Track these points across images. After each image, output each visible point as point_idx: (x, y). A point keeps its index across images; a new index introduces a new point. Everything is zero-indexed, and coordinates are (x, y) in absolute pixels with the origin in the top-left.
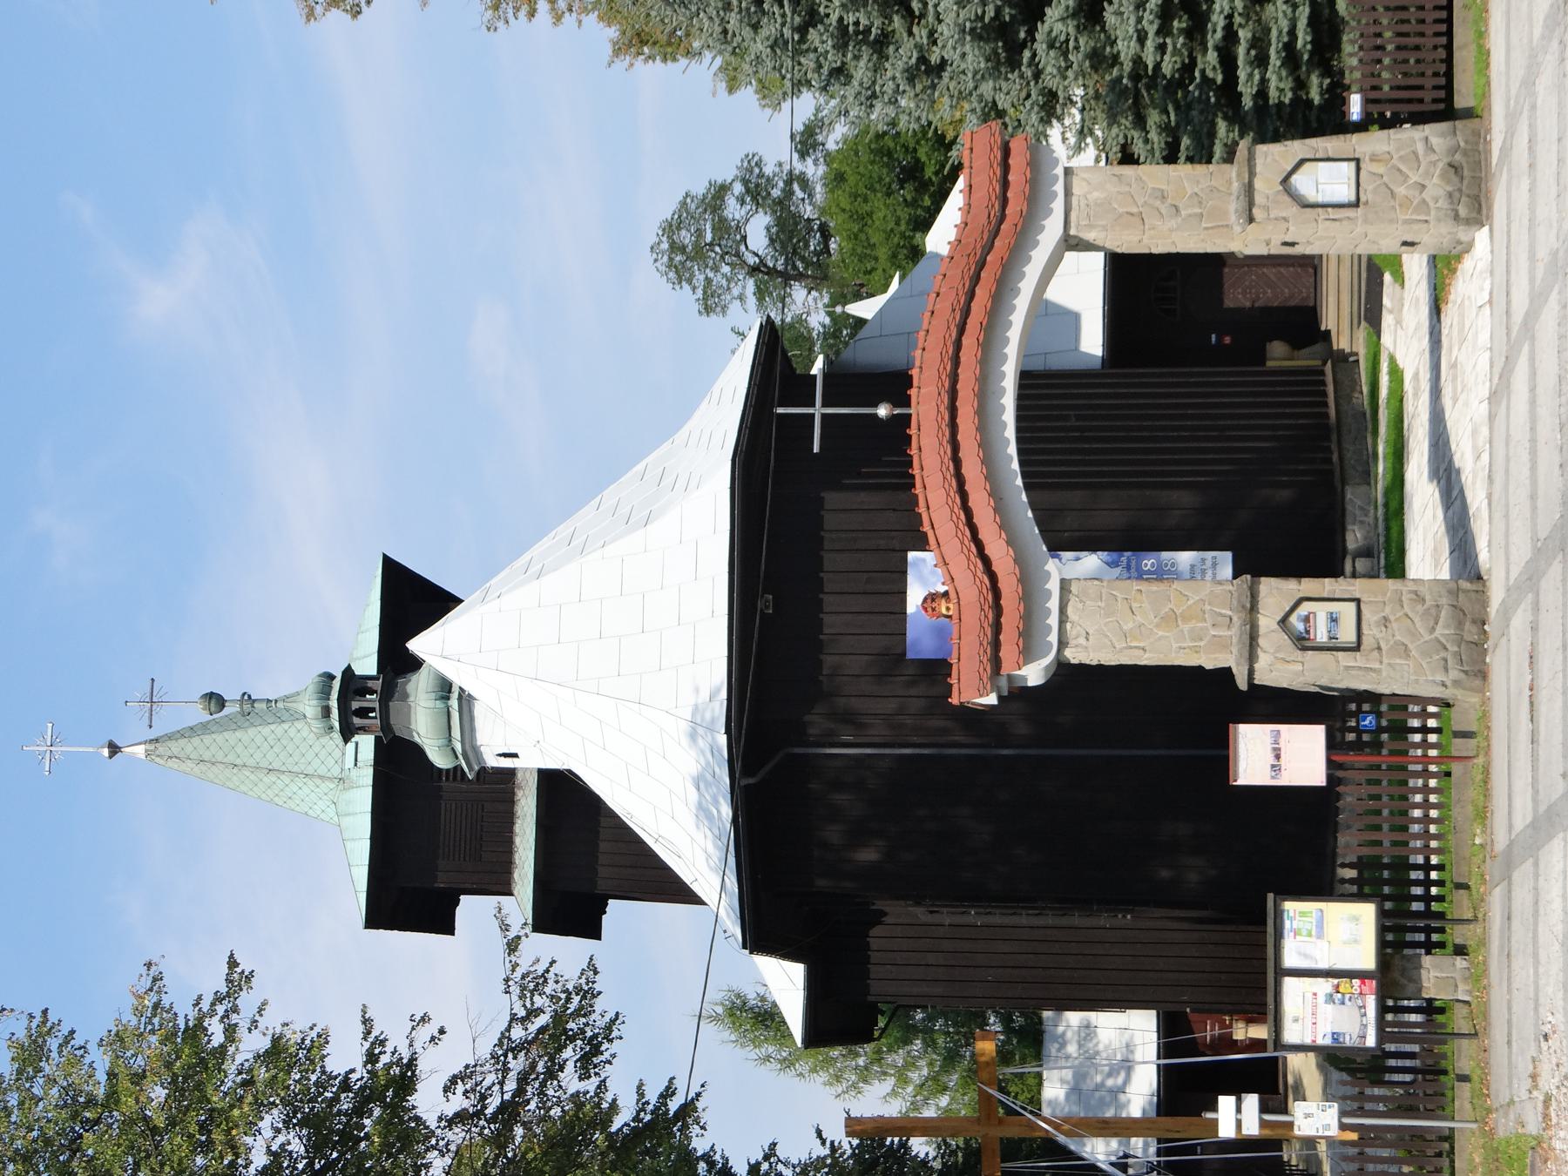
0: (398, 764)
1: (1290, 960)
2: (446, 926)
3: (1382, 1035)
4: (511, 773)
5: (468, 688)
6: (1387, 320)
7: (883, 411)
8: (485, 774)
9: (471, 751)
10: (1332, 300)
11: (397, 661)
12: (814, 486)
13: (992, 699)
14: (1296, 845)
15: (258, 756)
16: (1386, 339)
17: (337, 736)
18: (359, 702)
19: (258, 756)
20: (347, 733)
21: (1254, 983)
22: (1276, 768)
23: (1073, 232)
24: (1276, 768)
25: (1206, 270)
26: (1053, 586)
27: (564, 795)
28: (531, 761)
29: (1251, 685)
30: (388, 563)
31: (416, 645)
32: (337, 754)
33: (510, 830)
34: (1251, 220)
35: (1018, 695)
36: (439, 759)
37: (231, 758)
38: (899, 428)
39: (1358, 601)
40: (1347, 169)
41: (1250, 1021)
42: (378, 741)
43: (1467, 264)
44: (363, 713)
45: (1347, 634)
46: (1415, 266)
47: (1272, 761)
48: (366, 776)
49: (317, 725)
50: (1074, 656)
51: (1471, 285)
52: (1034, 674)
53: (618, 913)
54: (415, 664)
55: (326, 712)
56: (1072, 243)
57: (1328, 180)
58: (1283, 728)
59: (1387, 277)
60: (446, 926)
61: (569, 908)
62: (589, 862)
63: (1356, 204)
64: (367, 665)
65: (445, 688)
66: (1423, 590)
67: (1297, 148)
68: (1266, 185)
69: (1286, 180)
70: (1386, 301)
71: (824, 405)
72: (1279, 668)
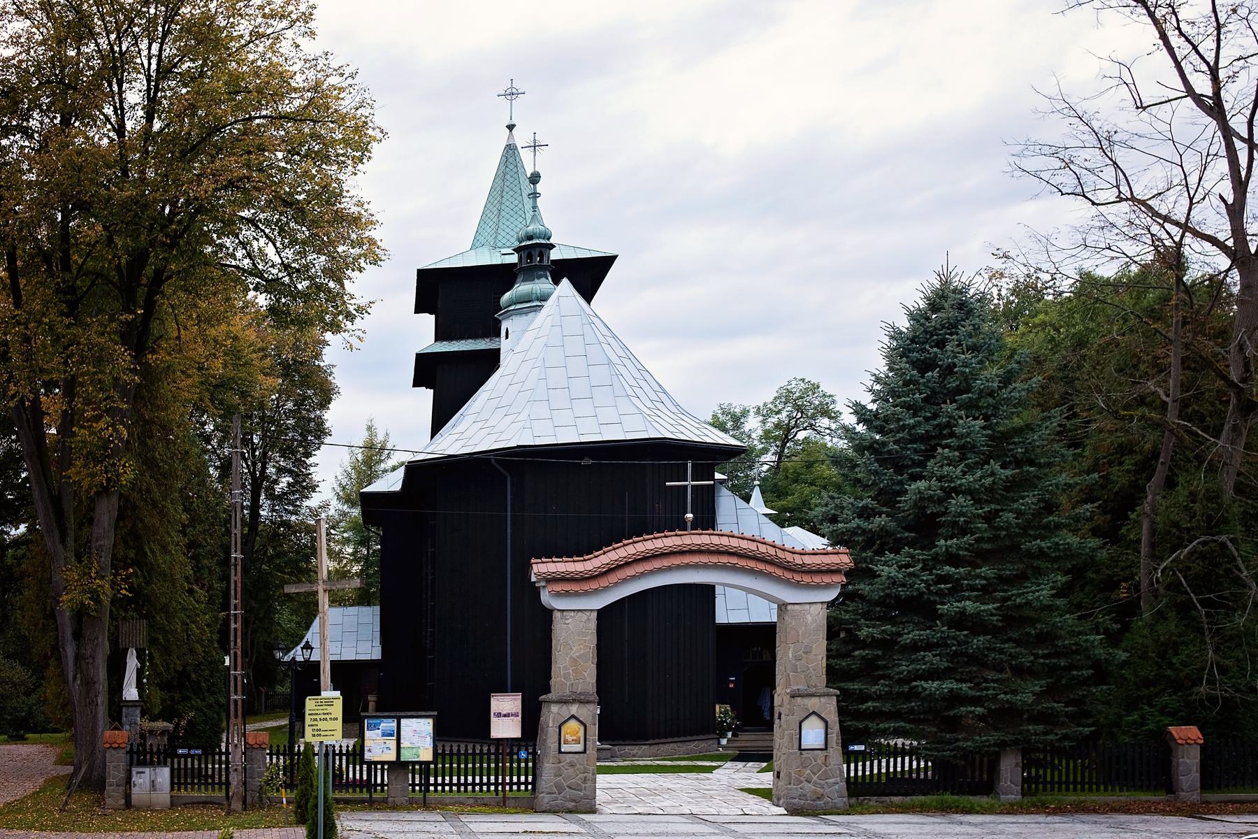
0: (502, 277)
1: (403, 721)
2: (419, 309)
3: (370, 764)
4: (499, 335)
5: (543, 310)
6: (740, 765)
7: (690, 516)
8: (497, 324)
9: (509, 314)
10: (753, 737)
11: (561, 270)
12: (645, 482)
13: (533, 579)
14: (462, 727)
15: (507, 203)
16: (729, 764)
17: (517, 244)
18: (535, 257)
19: (507, 203)
20: (517, 250)
21: (400, 704)
22: (499, 715)
23: (789, 607)
24: (499, 715)
25: (765, 677)
26: (239, 667)
27: (491, 361)
28: (504, 345)
29: (541, 702)
30: (613, 258)
31: (565, 282)
32: (508, 244)
33: (462, 338)
34: (793, 697)
35: (536, 592)
36: (506, 297)
37: (507, 189)
38: (682, 525)
39: (584, 752)
40: (819, 743)
41: (377, 702)
42: (514, 265)
43: (767, 803)
44: (530, 256)
45: (564, 748)
46: (767, 780)
47: (504, 712)
48: (497, 260)
49: (522, 234)
50: (557, 615)
51: (765, 807)
52: (546, 598)
53: (427, 395)
54: (556, 282)
55: (530, 238)
56: (782, 607)
57: (813, 735)
58: (519, 718)
59: (765, 764)
60: (419, 309)
61: (427, 370)
62: (450, 379)
63: (800, 749)
64: (555, 255)
65: (544, 298)
66: (589, 784)
67: (833, 718)
68: (813, 704)
69: (814, 713)
70: (751, 764)
71: (686, 486)
72: (552, 714)
